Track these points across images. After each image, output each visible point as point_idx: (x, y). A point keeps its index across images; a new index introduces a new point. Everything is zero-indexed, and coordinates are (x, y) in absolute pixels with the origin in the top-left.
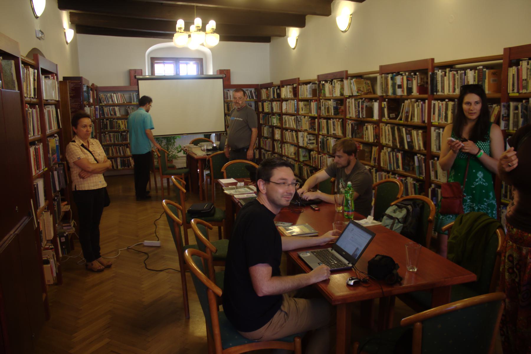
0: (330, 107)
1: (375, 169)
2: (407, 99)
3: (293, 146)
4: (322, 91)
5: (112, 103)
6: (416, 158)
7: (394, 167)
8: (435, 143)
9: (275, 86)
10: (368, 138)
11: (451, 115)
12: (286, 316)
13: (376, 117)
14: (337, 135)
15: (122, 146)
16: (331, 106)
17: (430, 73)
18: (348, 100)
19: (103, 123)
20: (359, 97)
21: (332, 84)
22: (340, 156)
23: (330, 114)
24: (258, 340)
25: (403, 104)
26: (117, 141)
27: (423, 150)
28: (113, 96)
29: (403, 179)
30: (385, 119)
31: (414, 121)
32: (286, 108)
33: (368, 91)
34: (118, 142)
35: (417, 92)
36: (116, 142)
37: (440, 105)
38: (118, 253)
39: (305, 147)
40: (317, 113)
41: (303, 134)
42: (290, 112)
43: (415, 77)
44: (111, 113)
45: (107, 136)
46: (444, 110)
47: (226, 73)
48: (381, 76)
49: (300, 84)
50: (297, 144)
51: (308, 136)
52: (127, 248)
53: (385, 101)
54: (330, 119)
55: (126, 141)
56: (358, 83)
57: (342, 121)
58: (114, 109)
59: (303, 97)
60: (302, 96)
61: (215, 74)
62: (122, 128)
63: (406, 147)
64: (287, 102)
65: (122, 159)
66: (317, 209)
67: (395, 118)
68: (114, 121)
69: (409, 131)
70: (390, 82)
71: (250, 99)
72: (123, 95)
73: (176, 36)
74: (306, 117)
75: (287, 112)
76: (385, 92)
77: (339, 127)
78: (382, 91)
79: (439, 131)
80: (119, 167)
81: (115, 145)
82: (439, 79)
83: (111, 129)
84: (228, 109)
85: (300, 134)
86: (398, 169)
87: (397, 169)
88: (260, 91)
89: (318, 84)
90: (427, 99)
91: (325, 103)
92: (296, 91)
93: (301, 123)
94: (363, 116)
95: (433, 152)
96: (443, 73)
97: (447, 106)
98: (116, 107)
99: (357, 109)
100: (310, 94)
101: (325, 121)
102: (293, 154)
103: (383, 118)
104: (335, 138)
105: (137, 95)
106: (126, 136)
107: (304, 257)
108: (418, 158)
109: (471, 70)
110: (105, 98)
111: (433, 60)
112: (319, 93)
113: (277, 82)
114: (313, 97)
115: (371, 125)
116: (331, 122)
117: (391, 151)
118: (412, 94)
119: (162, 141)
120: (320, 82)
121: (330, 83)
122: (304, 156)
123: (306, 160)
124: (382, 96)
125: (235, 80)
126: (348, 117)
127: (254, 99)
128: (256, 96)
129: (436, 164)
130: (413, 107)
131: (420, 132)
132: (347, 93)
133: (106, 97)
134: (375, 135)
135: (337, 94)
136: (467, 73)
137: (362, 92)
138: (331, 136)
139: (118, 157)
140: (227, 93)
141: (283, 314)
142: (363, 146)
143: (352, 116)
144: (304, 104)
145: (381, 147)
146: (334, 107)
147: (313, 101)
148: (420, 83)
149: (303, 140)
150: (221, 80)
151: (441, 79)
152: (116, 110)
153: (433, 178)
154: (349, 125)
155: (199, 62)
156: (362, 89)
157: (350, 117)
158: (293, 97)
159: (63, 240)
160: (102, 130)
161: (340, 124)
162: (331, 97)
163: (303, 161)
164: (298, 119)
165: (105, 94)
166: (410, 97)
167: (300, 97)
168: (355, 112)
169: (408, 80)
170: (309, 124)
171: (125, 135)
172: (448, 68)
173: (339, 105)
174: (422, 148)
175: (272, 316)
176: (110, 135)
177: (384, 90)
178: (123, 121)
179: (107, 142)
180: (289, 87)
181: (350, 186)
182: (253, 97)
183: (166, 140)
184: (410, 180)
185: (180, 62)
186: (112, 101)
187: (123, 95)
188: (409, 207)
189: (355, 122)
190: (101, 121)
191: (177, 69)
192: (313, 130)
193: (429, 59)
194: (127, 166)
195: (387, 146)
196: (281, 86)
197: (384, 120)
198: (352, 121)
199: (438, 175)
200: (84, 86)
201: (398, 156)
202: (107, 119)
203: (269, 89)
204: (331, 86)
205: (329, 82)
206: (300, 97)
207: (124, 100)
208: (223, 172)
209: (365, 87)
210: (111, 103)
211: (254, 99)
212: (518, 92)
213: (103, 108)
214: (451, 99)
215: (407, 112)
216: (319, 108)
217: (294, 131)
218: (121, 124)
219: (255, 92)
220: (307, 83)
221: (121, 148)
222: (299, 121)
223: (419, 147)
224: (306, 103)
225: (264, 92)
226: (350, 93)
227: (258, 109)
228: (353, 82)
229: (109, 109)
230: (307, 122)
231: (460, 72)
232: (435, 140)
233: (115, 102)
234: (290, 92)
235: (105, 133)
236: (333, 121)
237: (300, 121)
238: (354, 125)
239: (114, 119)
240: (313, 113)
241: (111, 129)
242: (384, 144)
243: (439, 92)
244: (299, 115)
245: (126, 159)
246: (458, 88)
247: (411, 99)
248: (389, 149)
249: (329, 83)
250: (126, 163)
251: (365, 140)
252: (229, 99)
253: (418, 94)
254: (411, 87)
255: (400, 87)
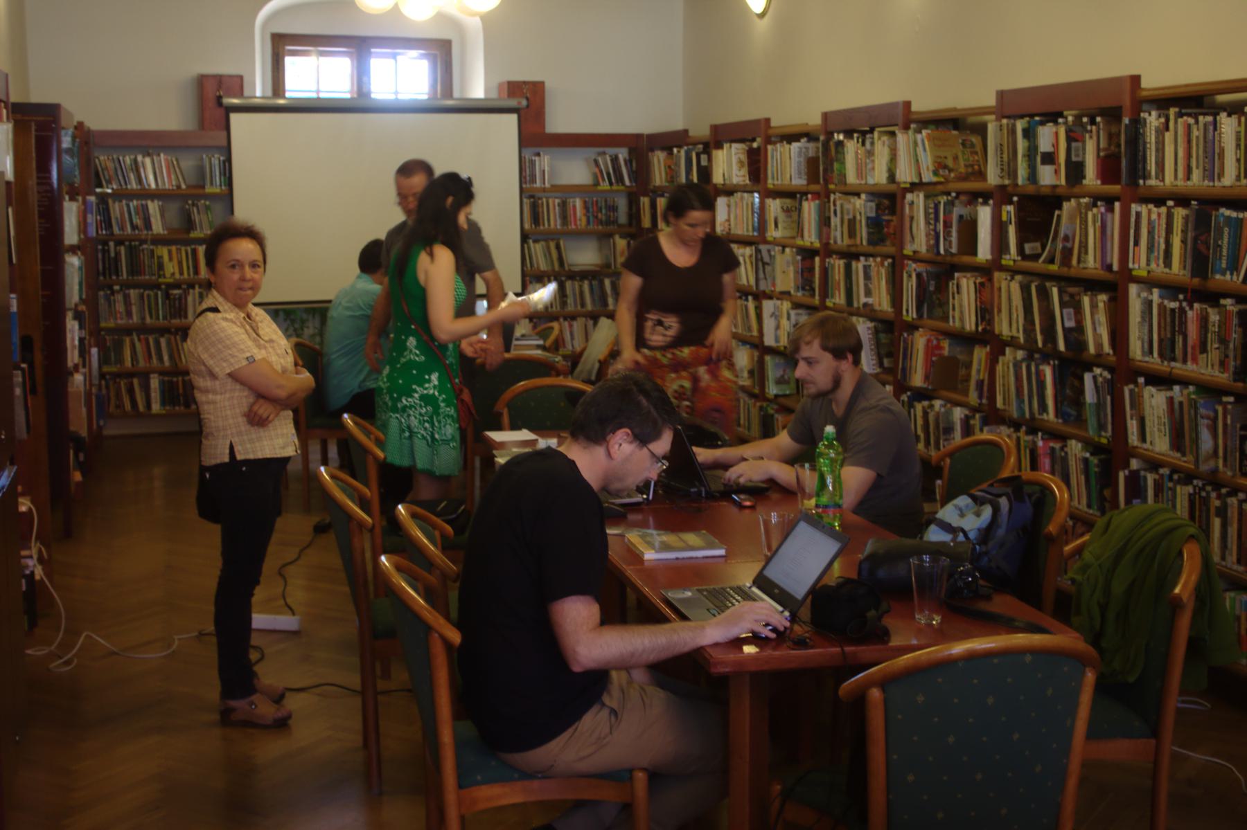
0: (858, 217)
1: (981, 417)
2: (1068, 199)
3: (748, 346)
4: (836, 165)
5: (139, 187)
6: (1088, 377)
7: (1029, 408)
8: (1139, 332)
9: (695, 144)
10: (962, 320)
11: (1181, 247)
12: (613, 718)
13: (984, 252)
14: (875, 311)
15: (166, 336)
16: (860, 214)
17: (1126, 120)
18: (909, 197)
19: (107, 255)
20: (940, 188)
21: (863, 144)
22: (810, 358)
23: (858, 242)
24: (544, 774)
25: (1057, 212)
26: (151, 317)
27: (1108, 354)
28: (143, 163)
29: (1057, 446)
30: (1010, 259)
31: (1085, 266)
32: (725, 217)
33: (970, 170)
34: (153, 321)
35: (1098, 178)
36: (148, 320)
37: (1154, 216)
38: (170, 646)
39: (782, 348)
40: (820, 236)
41: (776, 307)
42: (739, 232)
43: (1091, 131)
44: (134, 221)
46: (1163, 234)
47: (528, 95)
48: (998, 123)
49: (773, 139)
50: (757, 341)
51: (793, 313)
52: (196, 634)
53: (1011, 203)
54: (856, 256)
55: (180, 317)
56: (936, 143)
57: (893, 265)
58: (145, 208)
59: (779, 182)
60: (777, 179)
61: (494, 95)
62: (168, 275)
63: (1062, 346)
64: (732, 197)
65: (166, 379)
66: (748, 503)
67: (1035, 257)
68: (143, 250)
69: (1072, 296)
70: (1021, 144)
71: (611, 184)
72: (175, 163)
74: (787, 250)
75: (729, 233)
76: (1009, 175)
77: (883, 283)
78: (1002, 169)
79: (1150, 298)
80: (156, 407)
81: (143, 330)
82: (1151, 138)
83: (133, 275)
84: (536, 218)
85: (768, 306)
86: (1045, 416)
87: (1040, 414)
88: (647, 156)
89: (823, 141)
90: (1118, 199)
91: (842, 206)
92: (759, 161)
93: (773, 270)
94: (951, 247)
95: (1133, 360)
96: (1163, 120)
97: (1170, 217)
98: (153, 201)
99: (932, 227)
100: (800, 173)
101: (842, 262)
102: (746, 374)
103: (1005, 254)
104: (872, 319)
105: (224, 162)
106: (183, 301)
107: (673, 598)
108: (1095, 378)
109: (1229, 115)
110: (116, 169)
111: (1136, 80)
112: (825, 170)
113: (701, 130)
114: (808, 184)
115: (968, 279)
116: (859, 266)
117: (1023, 360)
118: (1084, 182)
119: (303, 322)
120: (830, 135)
121: (860, 140)
122: (780, 381)
123: (788, 392)
124: (1002, 188)
125: (559, 121)
126: (908, 251)
127: (623, 184)
128: (634, 175)
129: (1143, 397)
130: (1084, 222)
131: (1102, 298)
132: (905, 175)
133: (118, 166)
134: (981, 307)
135: (879, 177)
136: (1221, 124)
137: (950, 170)
138: (858, 314)
139: (154, 372)
140: (533, 163)
141: (605, 713)
142: (950, 345)
143: (918, 249)
144: (782, 208)
145: (998, 346)
146: (868, 218)
147: (810, 196)
148: (1104, 150)
149: (778, 327)
150: (513, 119)
151: (1157, 138)
152: (151, 211)
153: (1133, 439)
154: (910, 276)
155: (437, 53)
156: (950, 163)
157: (915, 252)
158: (748, 182)
160: (101, 278)
161: (888, 274)
162: (861, 184)
163: (776, 396)
164: (762, 257)
165: (115, 156)
166: (1076, 190)
167: (771, 183)
168: (927, 235)
169: (1070, 139)
170: (796, 272)
171: (180, 299)
172: (1174, 106)
173: (887, 212)
174: (1107, 349)
175: (577, 716)
176: (127, 298)
177: (1005, 168)
178: (174, 248)
179: (116, 319)
180: (737, 149)
181: (831, 437)
182: (620, 179)
183: (318, 318)
184: (1075, 448)
185: (373, 50)
187: (177, 160)
188: (1004, 502)
189: (929, 268)
190: (100, 247)
191: (361, 74)
192: (807, 293)
193: (1126, 77)
194: (182, 402)
195: (1013, 343)
196: (712, 145)
197: (1007, 261)
198: (919, 264)
199: (1148, 429)
200: (63, 132)
201: (1045, 376)
202: (120, 242)
203: (675, 150)
204: (863, 148)
205: (855, 135)
206: (771, 183)
207: (179, 180)
208: (501, 414)
209: (960, 154)
210: (135, 186)
211: (627, 187)
213: (107, 204)
214: (1182, 200)
215: (1066, 238)
216: (824, 222)
217: (750, 298)
218: (166, 258)
219: (628, 162)
220: (791, 137)
221: (163, 341)
222: (764, 264)
223: (1099, 345)
224: (788, 201)
225: (659, 161)
226: (914, 176)
227: (639, 220)
228: (923, 141)
229: (125, 209)
230: (788, 266)
231: (1204, 118)
232: (1139, 323)
233: (149, 185)
234: (741, 162)
235: (110, 287)
236: (868, 263)
237: (768, 264)
238: (926, 278)
239: (143, 242)
240: (810, 236)
241: (133, 275)
242: (1004, 338)
243: (1150, 177)
244: (766, 242)
245: (180, 378)
246: (1197, 168)
247: (1078, 197)
248: (1020, 354)
249: (858, 138)
250: (181, 391)
251: (951, 323)
252: (538, 184)
253: (1099, 182)
254: (1080, 159)
255: (1049, 158)
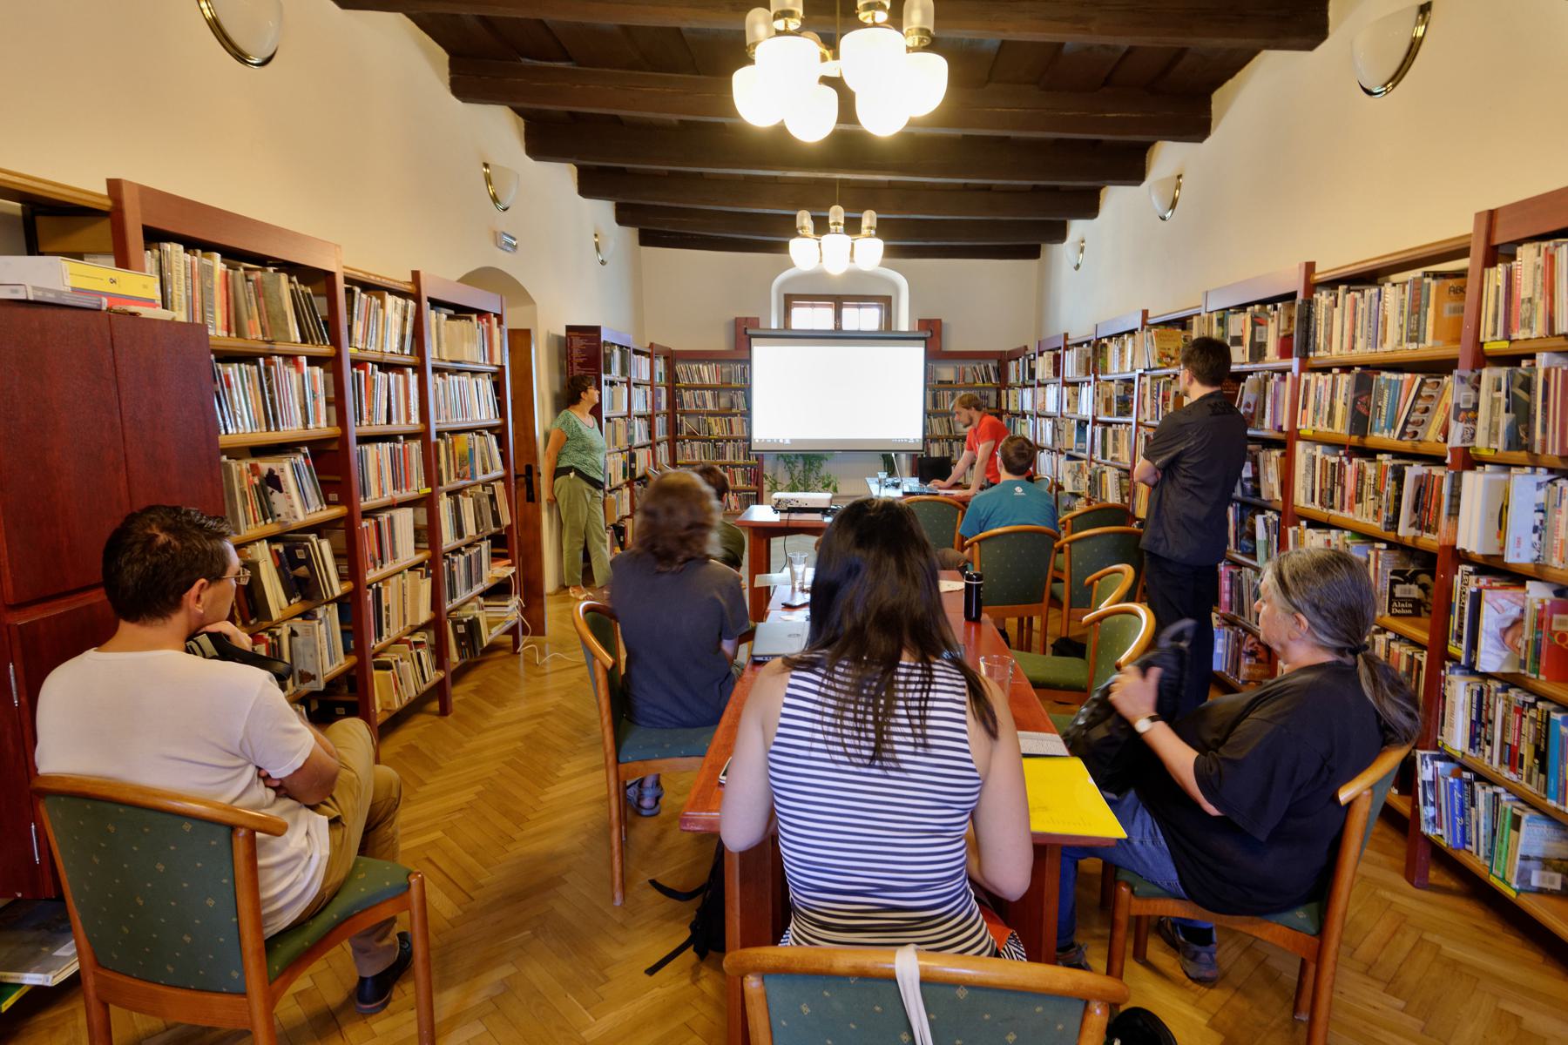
45: (688, 446)
46: (1328, 398)
58: (703, 396)
71: (984, 382)
73: (795, 244)
79: (1314, 454)
84: (935, 404)
96: (1332, 298)
148: (1284, 331)
159: (461, 629)
178: (718, 418)
186: (701, 378)
212: (1507, 337)
222: (1059, 430)
